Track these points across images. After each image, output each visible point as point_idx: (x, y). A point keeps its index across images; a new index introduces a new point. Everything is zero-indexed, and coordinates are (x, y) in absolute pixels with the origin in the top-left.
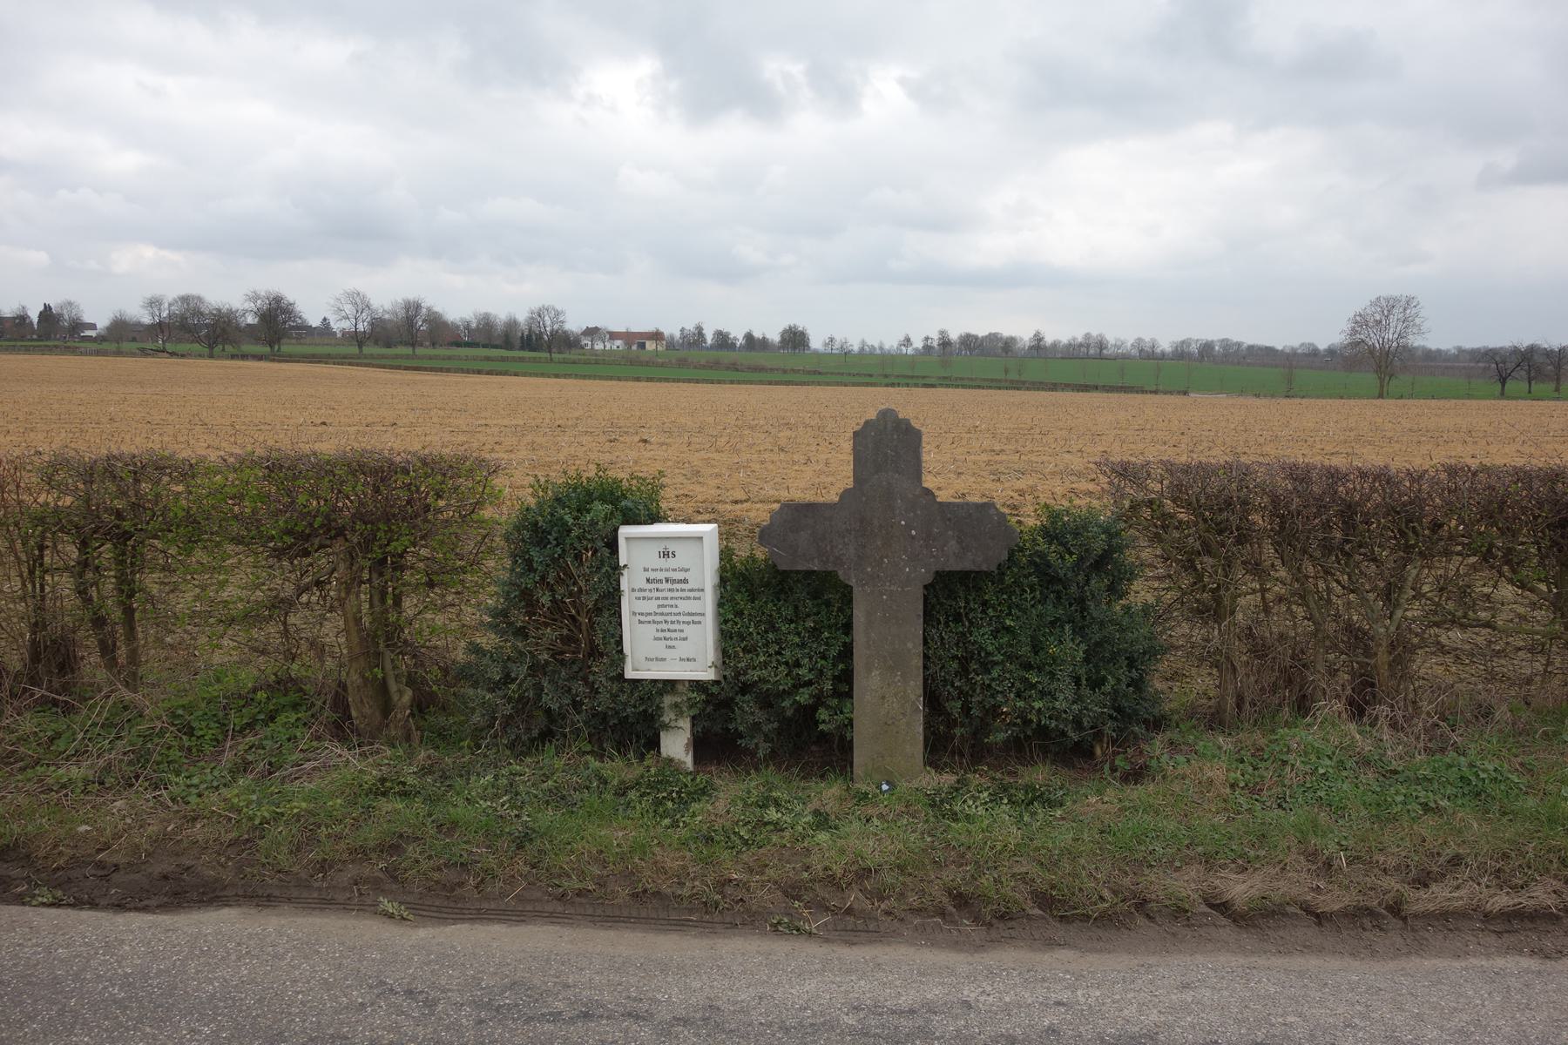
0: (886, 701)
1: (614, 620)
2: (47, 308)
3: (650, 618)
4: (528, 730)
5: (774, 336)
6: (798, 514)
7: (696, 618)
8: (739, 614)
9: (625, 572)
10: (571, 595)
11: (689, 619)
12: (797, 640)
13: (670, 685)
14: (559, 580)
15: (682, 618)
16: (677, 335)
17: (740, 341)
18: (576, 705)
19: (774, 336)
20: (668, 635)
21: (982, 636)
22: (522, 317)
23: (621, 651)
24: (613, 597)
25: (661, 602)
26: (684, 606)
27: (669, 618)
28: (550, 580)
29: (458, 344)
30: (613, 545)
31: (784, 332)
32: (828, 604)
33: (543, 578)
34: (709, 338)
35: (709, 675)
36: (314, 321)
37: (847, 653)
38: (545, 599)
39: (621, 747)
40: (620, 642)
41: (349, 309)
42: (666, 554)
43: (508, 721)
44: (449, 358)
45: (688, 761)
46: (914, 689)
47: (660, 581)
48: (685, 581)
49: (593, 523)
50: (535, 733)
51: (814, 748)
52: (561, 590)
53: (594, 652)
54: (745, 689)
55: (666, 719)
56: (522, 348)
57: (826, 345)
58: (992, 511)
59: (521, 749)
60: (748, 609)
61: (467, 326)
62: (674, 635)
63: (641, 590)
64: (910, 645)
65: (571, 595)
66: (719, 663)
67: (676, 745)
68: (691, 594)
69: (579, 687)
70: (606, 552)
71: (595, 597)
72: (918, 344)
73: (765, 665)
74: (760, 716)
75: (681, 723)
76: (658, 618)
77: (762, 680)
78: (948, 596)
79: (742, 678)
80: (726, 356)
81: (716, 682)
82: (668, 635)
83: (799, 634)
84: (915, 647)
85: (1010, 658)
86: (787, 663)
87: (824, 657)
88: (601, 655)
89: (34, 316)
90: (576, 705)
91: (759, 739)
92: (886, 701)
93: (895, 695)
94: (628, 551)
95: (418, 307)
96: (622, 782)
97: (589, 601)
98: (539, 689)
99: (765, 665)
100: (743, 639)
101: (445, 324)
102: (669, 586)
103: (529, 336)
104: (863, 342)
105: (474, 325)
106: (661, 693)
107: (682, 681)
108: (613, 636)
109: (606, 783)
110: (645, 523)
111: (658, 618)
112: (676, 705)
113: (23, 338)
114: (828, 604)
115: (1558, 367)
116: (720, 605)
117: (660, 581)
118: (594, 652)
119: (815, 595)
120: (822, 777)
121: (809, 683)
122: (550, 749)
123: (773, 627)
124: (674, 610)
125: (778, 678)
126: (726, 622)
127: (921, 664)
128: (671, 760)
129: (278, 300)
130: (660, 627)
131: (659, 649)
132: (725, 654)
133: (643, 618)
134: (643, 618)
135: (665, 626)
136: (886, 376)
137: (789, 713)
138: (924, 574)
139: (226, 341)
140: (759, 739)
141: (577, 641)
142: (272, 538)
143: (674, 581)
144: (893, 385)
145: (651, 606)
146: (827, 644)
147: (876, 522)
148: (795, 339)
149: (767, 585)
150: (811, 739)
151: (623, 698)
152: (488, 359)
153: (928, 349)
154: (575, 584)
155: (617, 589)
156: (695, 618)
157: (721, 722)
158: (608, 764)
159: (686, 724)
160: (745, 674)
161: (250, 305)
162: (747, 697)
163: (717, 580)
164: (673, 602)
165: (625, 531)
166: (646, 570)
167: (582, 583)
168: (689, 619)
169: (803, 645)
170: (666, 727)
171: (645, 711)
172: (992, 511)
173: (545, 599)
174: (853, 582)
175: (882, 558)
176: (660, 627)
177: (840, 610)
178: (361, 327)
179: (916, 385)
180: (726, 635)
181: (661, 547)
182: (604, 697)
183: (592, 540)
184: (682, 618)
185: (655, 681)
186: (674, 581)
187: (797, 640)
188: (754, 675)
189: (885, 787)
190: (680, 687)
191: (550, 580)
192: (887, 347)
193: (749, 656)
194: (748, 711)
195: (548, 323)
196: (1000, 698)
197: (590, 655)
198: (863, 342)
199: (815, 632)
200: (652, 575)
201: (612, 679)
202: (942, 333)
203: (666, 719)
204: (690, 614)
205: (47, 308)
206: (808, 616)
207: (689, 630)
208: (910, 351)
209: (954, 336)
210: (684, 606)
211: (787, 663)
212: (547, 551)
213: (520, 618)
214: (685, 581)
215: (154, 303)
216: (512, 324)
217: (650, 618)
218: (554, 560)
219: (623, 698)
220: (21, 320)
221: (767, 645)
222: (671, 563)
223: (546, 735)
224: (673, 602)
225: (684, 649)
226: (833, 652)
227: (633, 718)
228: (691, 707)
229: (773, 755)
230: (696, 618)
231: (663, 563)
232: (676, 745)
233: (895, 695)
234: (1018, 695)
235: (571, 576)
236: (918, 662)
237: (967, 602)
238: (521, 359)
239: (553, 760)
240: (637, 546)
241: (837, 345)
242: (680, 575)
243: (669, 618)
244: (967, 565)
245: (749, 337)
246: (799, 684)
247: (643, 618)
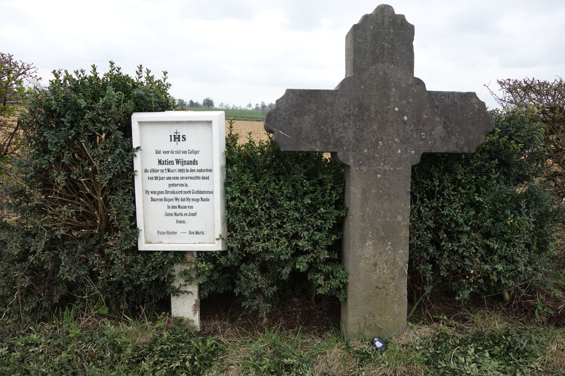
0: (376, 264)
1: (127, 197)
3: (161, 196)
4: (51, 296)
5: (201, 102)
6: (300, 101)
7: (205, 196)
8: (245, 192)
9: (138, 154)
10: (87, 175)
11: (198, 196)
12: (297, 215)
13: (180, 255)
14: (74, 162)
15: (191, 196)
17: (188, 103)
18: (93, 275)
19: (201, 102)
20: (178, 211)
21: (454, 211)
23: (135, 226)
24: (125, 179)
25: (172, 182)
26: (194, 185)
27: (179, 196)
28: (65, 160)
30: (126, 130)
31: (205, 100)
32: (321, 183)
33: (58, 160)
35: (217, 247)
37: (340, 225)
38: (60, 179)
39: (135, 313)
40: (133, 218)
42: (176, 138)
43: (28, 292)
45: (196, 319)
46: (402, 256)
47: (171, 163)
48: (195, 162)
49: (107, 107)
50: (56, 299)
51: (295, 300)
52: (76, 170)
53: (110, 228)
54: (248, 258)
55: (176, 285)
57: (220, 106)
58: (474, 101)
59: (41, 315)
60: (253, 188)
62: (183, 211)
63: (153, 171)
64: (400, 218)
65: (87, 175)
66: (225, 237)
67: (185, 307)
68: (200, 174)
69: (95, 259)
70: (120, 134)
71: (109, 176)
72: (254, 107)
73: (268, 238)
74: (262, 281)
75: (190, 288)
76: (169, 196)
77: (266, 251)
78: (431, 172)
79: (247, 249)
81: (223, 253)
82: (178, 211)
83: (297, 210)
84: (402, 218)
85: (476, 229)
86: (287, 236)
87: (319, 230)
88: (117, 230)
90: (93, 275)
91: (259, 301)
92: (376, 264)
93: (386, 262)
94: (141, 136)
96: (136, 349)
97: (103, 180)
98: (57, 261)
99: (268, 238)
100: (248, 214)
102: (180, 167)
104: (234, 106)
106: (171, 263)
107: (192, 252)
108: (127, 212)
109: (120, 351)
110: (156, 110)
111: (169, 196)
112: (185, 273)
114: (321, 183)
116: (227, 184)
117: (171, 163)
118: (110, 228)
119: (310, 175)
121: (308, 252)
122: (68, 314)
123: (275, 204)
124: (184, 189)
125: (283, 249)
126: (233, 199)
127: (408, 235)
128: (181, 320)
130: (171, 204)
131: (170, 224)
132: (230, 227)
133: (155, 196)
134: (155, 196)
135: (175, 203)
136: (242, 117)
137: (285, 278)
138: (413, 156)
140: (259, 301)
141: (94, 218)
143: (184, 163)
144: (245, 120)
145: (163, 185)
146: (322, 218)
147: (373, 109)
149: (268, 167)
150: (310, 300)
151: (137, 268)
153: (257, 108)
154: (90, 164)
155: (131, 171)
156: (203, 196)
157: (223, 283)
158: (123, 327)
159: (194, 289)
160: (250, 245)
162: (251, 266)
163: (224, 163)
164: (183, 182)
165: (136, 117)
166: (158, 152)
167: (96, 164)
168: (198, 196)
169: (301, 220)
170: (177, 292)
171: (158, 280)
172: (474, 101)
173: (60, 179)
174: (351, 162)
175: (377, 140)
176: (171, 204)
177: (333, 188)
179: (254, 121)
180: (231, 209)
181: (172, 130)
182: (118, 268)
183: (106, 123)
184: (191, 196)
185: (166, 253)
186: (184, 163)
187: (297, 215)
188: (259, 246)
189: (379, 344)
190: (189, 257)
191: (65, 160)
192: (242, 107)
193: (253, 230)
194: (252, 277)
196: (467, 262)
197: (106, 230)
198: (234, 106)
199: (312, 209)
200: (163, 157)
201: (126, 252)
202: (262, 102)
203: (176, 285)
204: (199, 192)
206: (305, 194)
207: (198, 207)
208: (251, 109)
209: (267, 104)
210: (194, 185)
211: (287, 236)
212: (61, 134)
213: (38, 197)
214: (195, 162)
217: (161, 196)
218: (67, 141)
219: (137, 268)
221: (269, 220)
222: (181, 146)
223: (67, 301)
224: (183, 182)
225: (192, 224)
226: (328, 226)
227: (147, 283)
228: (199, 275)
229: (273, 318)
230: (205, 196)
231: (174, 146)
232: (185, 307)
233: (386, 262)
234: (482, 259)
235: (86, 158)
236: (405, 233)
237: (441, 181)
239: (71, 326)
240: (148, 134)
241: (224, 105)
242: (190, 157)
243: (179, 196)
244: (450, 148)
245: (191, 102)
246: (298, 252)
247: (155, 196)
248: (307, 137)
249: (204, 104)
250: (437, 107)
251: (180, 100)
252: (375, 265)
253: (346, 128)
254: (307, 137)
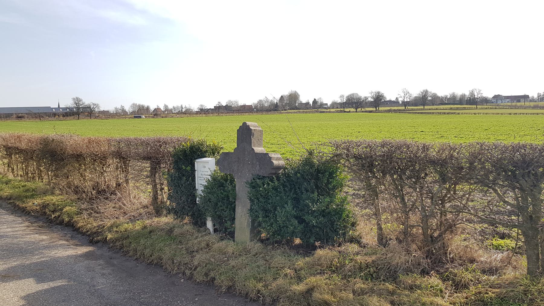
2: (315, 100)
16: (536, 96)
22: (467, 94)
29: (443, 104)
36: (393, 99)
41: (403, 95)
44: (437, 109)
56: (467, 104)
61: (446, 97)
89: (311, 103)
95: (426, 91)
101: (438, 97)
104: (406, 93)
105: (449, 97)
113: (308, 109)
120: (53, 140)
129: (379, 93)
139: (362, 107)
142: (281, 197)
152: (451, 109)
161: (370, 95)
178: (406, 100)
195: (476, 94)
205: (315, 100)
215: (342, 96)
216: (463, 96)
220: (308, 103)
238: (465, 109)
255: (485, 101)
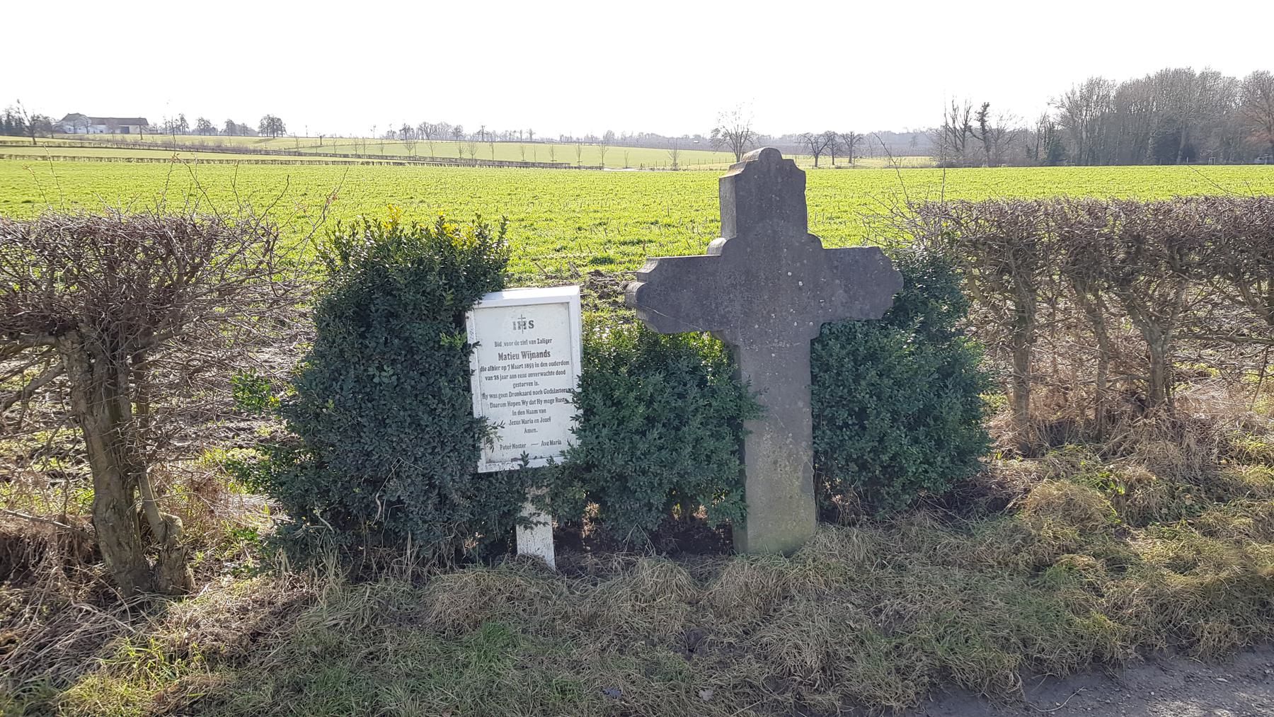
5: (254, 125)
17: (221, 126)
19: (254, 125)
34: (193, 125)
80: (210, 140)
103: (8, 122)
115: (851, 145)
138: (810, 328)
148: (274, 126)
172: (878, 256)
245: (230, 124)
248: (687, 315)
249: (263, 129)
250: (836, 267)
251: (201, 120)
252: (775, 462)
253: (731, 301)
254: (687, 315)
255: (40, 127)
